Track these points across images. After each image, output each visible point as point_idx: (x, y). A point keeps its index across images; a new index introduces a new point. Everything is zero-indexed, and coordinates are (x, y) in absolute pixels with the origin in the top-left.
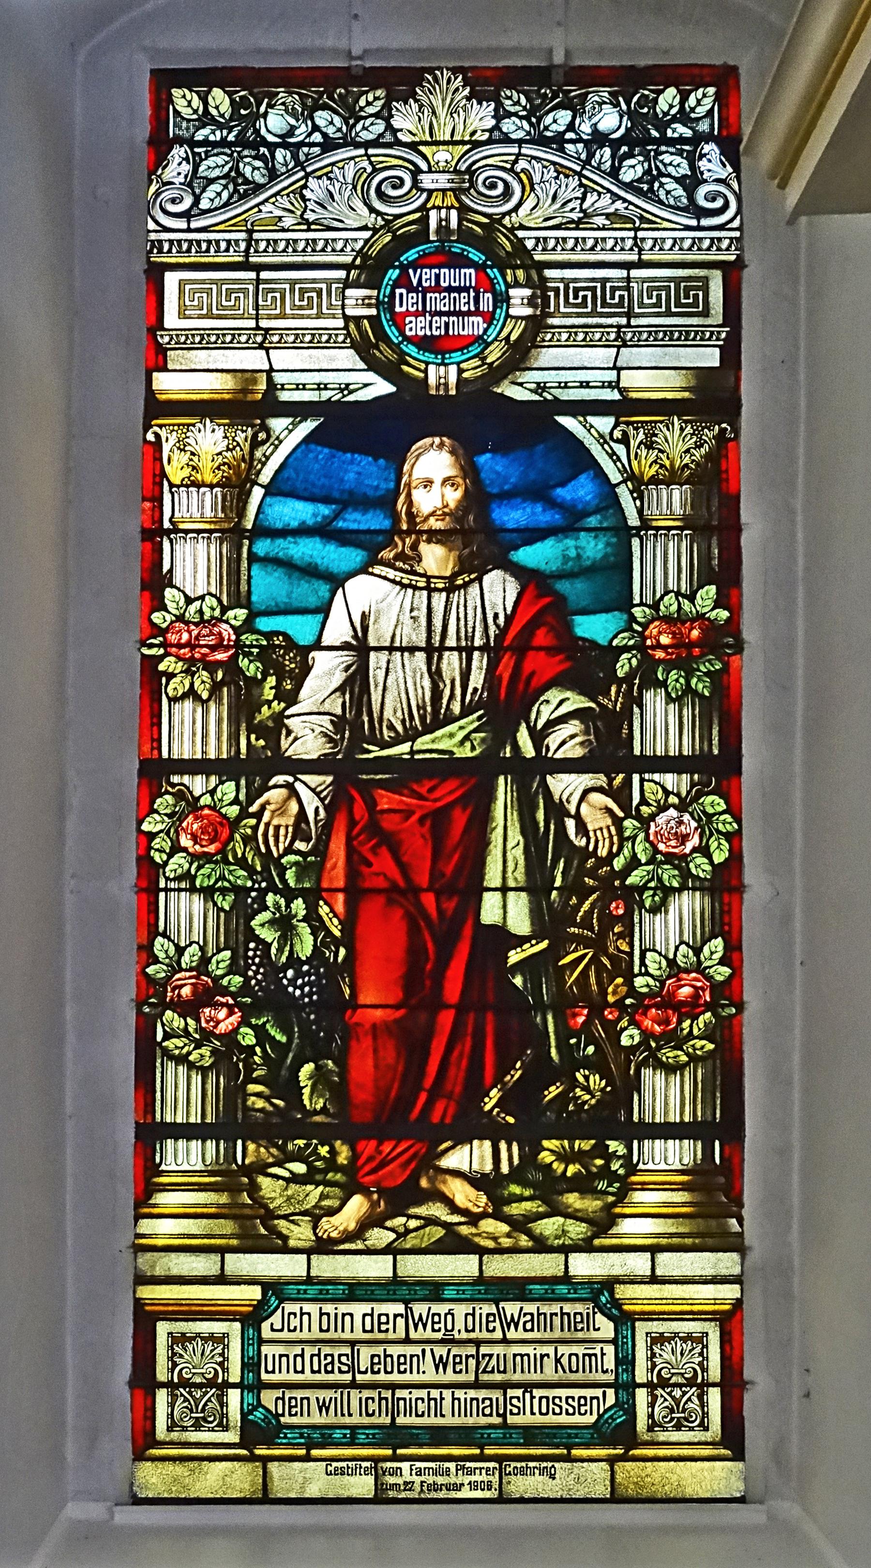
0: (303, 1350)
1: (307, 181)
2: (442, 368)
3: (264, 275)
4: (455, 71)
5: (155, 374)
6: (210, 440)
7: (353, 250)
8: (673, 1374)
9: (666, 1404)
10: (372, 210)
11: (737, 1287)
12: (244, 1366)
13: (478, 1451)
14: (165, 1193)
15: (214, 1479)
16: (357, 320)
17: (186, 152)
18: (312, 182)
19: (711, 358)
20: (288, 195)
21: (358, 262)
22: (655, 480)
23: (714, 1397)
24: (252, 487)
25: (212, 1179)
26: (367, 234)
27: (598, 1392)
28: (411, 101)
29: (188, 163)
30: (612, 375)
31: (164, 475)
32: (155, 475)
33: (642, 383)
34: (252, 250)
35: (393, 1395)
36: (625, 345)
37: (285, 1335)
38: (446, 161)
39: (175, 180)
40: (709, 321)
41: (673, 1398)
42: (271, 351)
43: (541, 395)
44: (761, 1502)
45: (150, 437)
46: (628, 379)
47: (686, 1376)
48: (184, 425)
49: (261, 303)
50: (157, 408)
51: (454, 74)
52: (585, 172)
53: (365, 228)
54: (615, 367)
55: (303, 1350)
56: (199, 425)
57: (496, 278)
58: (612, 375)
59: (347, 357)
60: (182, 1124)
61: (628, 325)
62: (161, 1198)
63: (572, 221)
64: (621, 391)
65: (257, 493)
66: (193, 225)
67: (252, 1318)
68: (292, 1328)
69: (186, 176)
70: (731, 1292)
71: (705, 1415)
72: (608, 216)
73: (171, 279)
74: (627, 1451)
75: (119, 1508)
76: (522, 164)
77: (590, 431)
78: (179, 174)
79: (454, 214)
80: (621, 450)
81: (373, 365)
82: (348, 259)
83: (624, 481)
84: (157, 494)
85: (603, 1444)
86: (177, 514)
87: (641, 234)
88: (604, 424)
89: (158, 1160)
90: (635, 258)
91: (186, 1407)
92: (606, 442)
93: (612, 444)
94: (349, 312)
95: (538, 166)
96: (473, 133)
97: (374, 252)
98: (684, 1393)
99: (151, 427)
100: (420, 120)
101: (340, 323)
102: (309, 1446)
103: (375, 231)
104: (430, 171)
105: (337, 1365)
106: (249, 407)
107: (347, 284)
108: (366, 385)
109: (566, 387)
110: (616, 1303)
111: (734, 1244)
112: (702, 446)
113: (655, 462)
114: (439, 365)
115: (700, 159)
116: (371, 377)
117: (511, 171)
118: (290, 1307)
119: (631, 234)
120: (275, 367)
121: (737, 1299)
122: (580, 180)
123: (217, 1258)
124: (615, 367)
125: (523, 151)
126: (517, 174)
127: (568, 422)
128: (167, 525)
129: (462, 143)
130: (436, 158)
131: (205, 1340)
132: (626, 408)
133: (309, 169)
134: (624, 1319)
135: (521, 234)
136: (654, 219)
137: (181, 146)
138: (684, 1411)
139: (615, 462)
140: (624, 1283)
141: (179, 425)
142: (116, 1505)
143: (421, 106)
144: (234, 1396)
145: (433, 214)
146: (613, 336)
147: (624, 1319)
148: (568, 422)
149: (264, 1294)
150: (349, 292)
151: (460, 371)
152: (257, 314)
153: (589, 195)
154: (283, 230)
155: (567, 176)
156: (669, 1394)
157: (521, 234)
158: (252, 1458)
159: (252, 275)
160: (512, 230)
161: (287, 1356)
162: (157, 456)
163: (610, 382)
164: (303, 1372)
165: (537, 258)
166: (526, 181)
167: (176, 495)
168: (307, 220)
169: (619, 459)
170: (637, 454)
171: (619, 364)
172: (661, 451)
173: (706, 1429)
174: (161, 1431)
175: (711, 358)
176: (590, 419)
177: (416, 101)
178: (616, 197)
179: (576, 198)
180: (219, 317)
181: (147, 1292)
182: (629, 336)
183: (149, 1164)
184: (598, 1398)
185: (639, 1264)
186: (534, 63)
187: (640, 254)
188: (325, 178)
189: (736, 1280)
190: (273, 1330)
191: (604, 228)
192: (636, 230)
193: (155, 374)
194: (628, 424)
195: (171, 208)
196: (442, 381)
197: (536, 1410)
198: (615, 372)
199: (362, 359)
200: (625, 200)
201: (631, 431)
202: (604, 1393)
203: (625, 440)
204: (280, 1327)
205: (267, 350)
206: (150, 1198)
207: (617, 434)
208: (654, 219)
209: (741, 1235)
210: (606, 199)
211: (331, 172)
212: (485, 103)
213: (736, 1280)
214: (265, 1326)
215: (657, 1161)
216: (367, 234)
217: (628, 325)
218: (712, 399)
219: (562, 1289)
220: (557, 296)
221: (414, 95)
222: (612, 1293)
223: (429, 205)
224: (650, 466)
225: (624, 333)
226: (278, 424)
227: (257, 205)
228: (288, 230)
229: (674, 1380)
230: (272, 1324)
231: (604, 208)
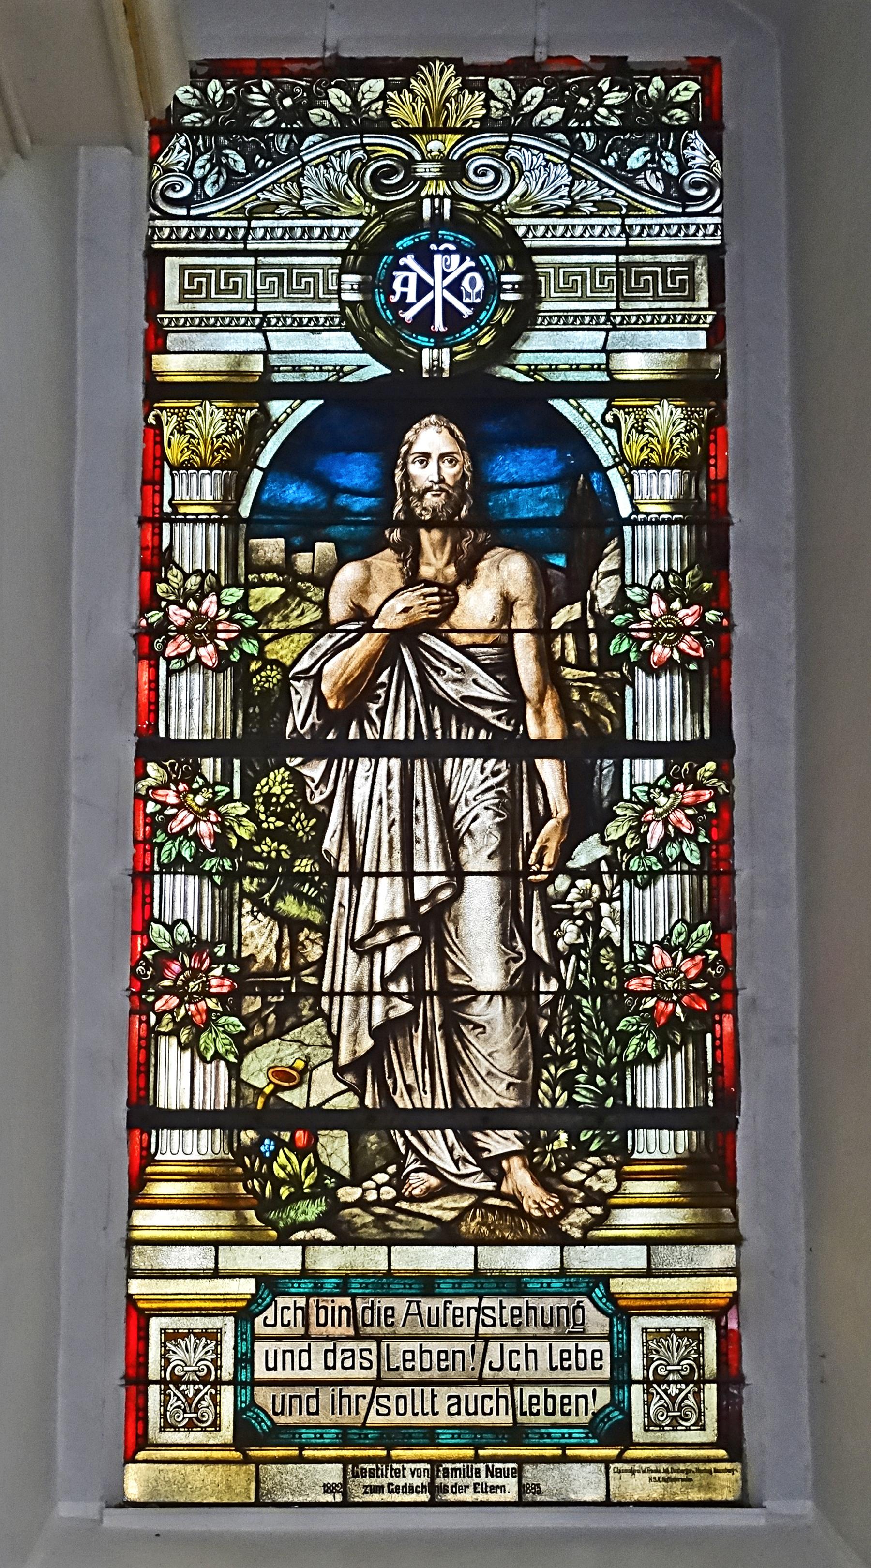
0: (309, 1345)
1: (304, 169)
2: (436, 351)
3: (262, 260)
4: (448, 61)
5: (154, 357)
6: (212, 420)
7: (347, 238)
8: (670, 1371)
9: (662, 1402)
10: (367, 198)
11: (734, 1279)
12: (237, 1362)
13: (384, 1453)
14: (157, 1184)
15: (204, 1482)
16: (352, 304)
17: (186, 141)
18: (310, 171)
19: (700, 340)
20: (317, 166)
21: (354, 247)
22: (646, 465)
23: (711, 1392)
24: (251, 471)
25: (201, 1169)
26: (361, 222)
27: (587, 1390)
28: (405, 90)
29: (188, 151)
30: (601, 358)
31: (164, 458)
32: (155, 459)
33: (634, 366)
34: (250, 237)
35: (374, 1391)
36: (615, 328)
37: (279, 1330)
38: (439, 151)
39: (175, 168)
40: (695, 305)
41: (669, 1396)
42: (268, 334)
43: (531, 377)
44: (760, 1506)
45: (151, 420)
46: (617, 361)
47: (683, 1373)
48: (184, 408)
49: (259, 287)
50: (157, 390)
51: (446, 64)
52: (573, 160)
53: (359, 217)
54: (604, 350)
55: (309, 1345)
56: (198, 408)
57: (488, 265)
58: (601, 358)
59: (347, 340)
60: (211, 1111)
61: (618, 309)
62: (158, 1189)
63: (560, 208)
64: (610, 375)
65: (256, 477)
66: (193, 212)
67: (245, 1314)
68: (286, 1322)
69: (186, 165)
70: (728, 1285)
71: (217, 1415)
72: (595, 203)
73: (171, 264)
74: (622, 1452)
75: (112, 1510)
76: (512, 152)
77: (585, 415)
78: (180, 162)
79: (447, 202)
80: (612, 434)
81: (368, 346)
82: (344, 246)
83: (616, 465)
84: (157, 478)
85: (601, 1444)
86: (177, 497)
87: (628, 221)
88: (596, 407)
89: (153, 1150)
90: (623, 244)
91: (179, 1407)
92: (598, 426)
93: (604, 428)
94: (345, 296)
95: (527, 154)
96: (467, 121)
97: (370, 237)
98: (681, 1391)
99: (152, 409)
100: (414, 110)
101: (335, 307)
102: (477, 1448)
103: (369, 219)
104: (424, 160)
105: (358, 1360)
106: (243, 390)
107: (343, 269)
108: (360, 367)
109: (557, 370)
110: (611, 1297)
111: (728, 1235)
112: (691, 430)
113: (646, 445)
114: (432, 348)
115: (684, 148)
116: (366, 358)
117: (502, 158)
118: (282, 1301)
119: (618, 221)
120: (274, 348)
121: (733, 1293)
122: (568, 168)
123: (210, 1250)
124: (604, 350)
125: (514, 139)
126: (508, 163)
127: (559, 405)
128: (167, 509)
129: (454, 131)
130: (430, 147)
131: (198, 1336)
132: (614, 389)
133: (306, 159)
134: (620, 1312)
135: (512, 221)
136: (640, 206)
137: (182, 135)
138: (196, 1412)
139: (607, 446)
140: (614, 1276)
141: (179, 408)
142: (107, 1507)
143: (415, 96)
144: (227, 1394)
145: (427, 203)
146: (603, 319)
147: (620, 1312)
148: (559, 405)
149: (258, 1287)
150: (344, 277)
151: (453, 354)
152: (256, 298)
153: (577, 182)
154: (281, 218)
155: (556, 164)
156: (665, 1391)
157: (512, 221)
158: (247, 1460)
159: (251, 261)
160: (502, 217)
161: (292, 1352)
162: (158, 439)
163: (599, 365)
164: (275, 1368)
165: (527, 244)
166: (515, 169)
167: (176, 478)
168: (303, 207)
169: (611, 443)
170: (628, 438)
171: (609, 348)
172: (651, 435)
173: (703, 1428)
174: (154, 1433)
175: (700, 340)
176: (583, 402)
177: (411, 91)
178: (602, 185)
179: (566, 185)
180: (280, 266)
181: (136, 1287)
182: (619, 319)
183: (144, 1153)
184: (585, 1397)
185: (636, 1257)
186: (523, 54)
187: (627, 241)
188: (322, 166)
189: (734, 1272)
190: (266, 1325)
191: (592, 215)
192: (623, 217)
193: (154, 357)
194: (619, 408)
195: (171, 194)
196: (436, 363)
197: (418, 1409)
198: (604, 355)
199: (358, 341)
200: (611, 188)
201: (621, 415)
202: (594, 1392)
203: (616, 425)
204: (273, 1322)
205: (264, 333)
206: (143, 1188)
207: (609, 418)
208: (640, 206)
209: (736, 1225)
210: (592, 187)
211: (327, 160)
212: (477, 93)
213: (734, 1272)
214: (259, 1321)
215: (652, 1150)
216: (361, 222)
217: (618, 309)
218: (696, 386)
219: (557, 1285)
220: (548, 282)
221: (407, 84)
222: (607, 1286)
223: (423, 194)
224: (642, 450)
225: (614, 317)
226: (277, 407)
227: (255, 193)
228: (286, 218)
229: (671, 1377)
230: (266, 1318)
231: (592, 195)
